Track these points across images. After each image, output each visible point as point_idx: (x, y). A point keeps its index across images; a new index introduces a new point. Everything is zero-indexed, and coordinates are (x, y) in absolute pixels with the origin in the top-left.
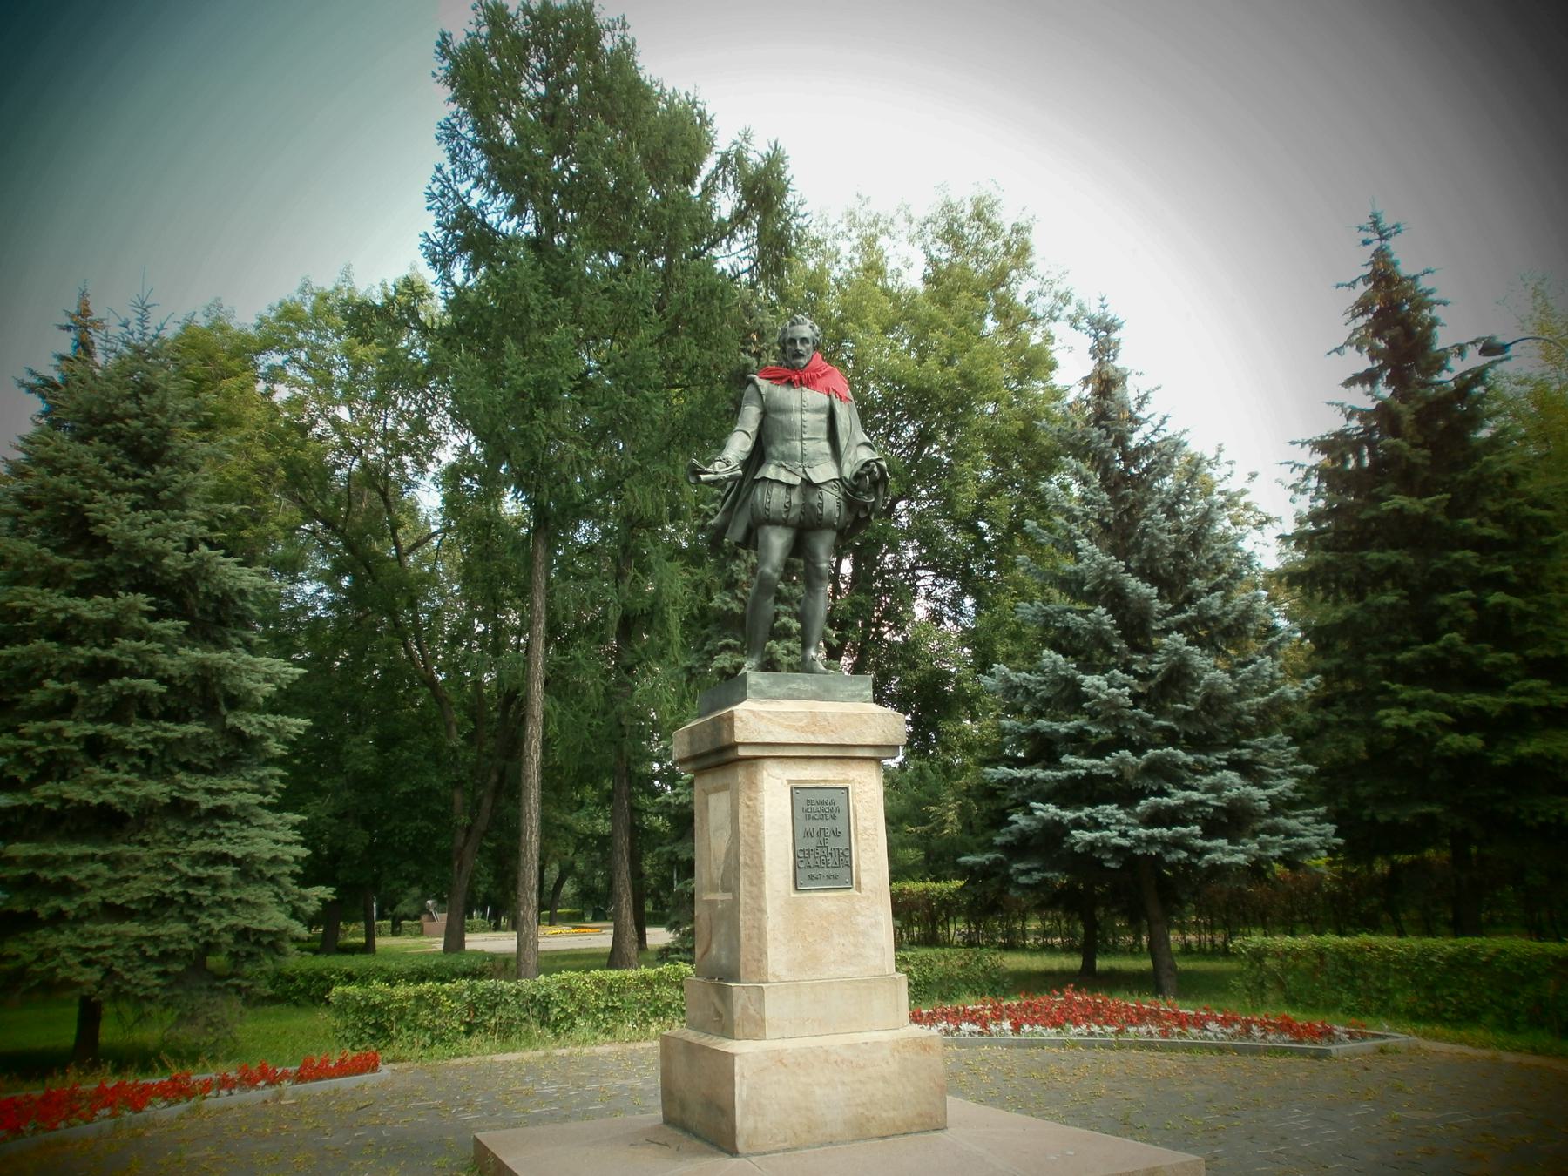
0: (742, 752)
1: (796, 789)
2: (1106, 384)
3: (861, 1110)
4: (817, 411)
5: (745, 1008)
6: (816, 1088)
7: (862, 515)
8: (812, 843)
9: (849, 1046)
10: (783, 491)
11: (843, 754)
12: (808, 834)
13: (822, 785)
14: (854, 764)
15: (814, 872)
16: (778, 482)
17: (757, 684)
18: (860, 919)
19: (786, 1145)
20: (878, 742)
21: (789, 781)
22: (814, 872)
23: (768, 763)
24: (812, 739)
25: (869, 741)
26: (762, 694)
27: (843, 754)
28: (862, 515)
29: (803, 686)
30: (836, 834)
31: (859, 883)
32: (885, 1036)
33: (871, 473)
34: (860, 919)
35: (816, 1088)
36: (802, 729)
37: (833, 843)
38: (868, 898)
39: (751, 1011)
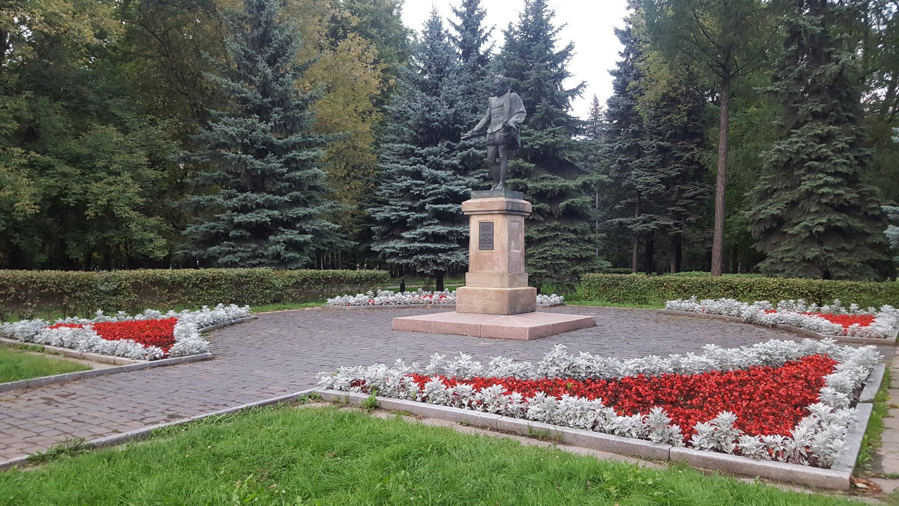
8: (483, 238)
26: (476, 198)
27: (490, 213)
37: (489, 238)
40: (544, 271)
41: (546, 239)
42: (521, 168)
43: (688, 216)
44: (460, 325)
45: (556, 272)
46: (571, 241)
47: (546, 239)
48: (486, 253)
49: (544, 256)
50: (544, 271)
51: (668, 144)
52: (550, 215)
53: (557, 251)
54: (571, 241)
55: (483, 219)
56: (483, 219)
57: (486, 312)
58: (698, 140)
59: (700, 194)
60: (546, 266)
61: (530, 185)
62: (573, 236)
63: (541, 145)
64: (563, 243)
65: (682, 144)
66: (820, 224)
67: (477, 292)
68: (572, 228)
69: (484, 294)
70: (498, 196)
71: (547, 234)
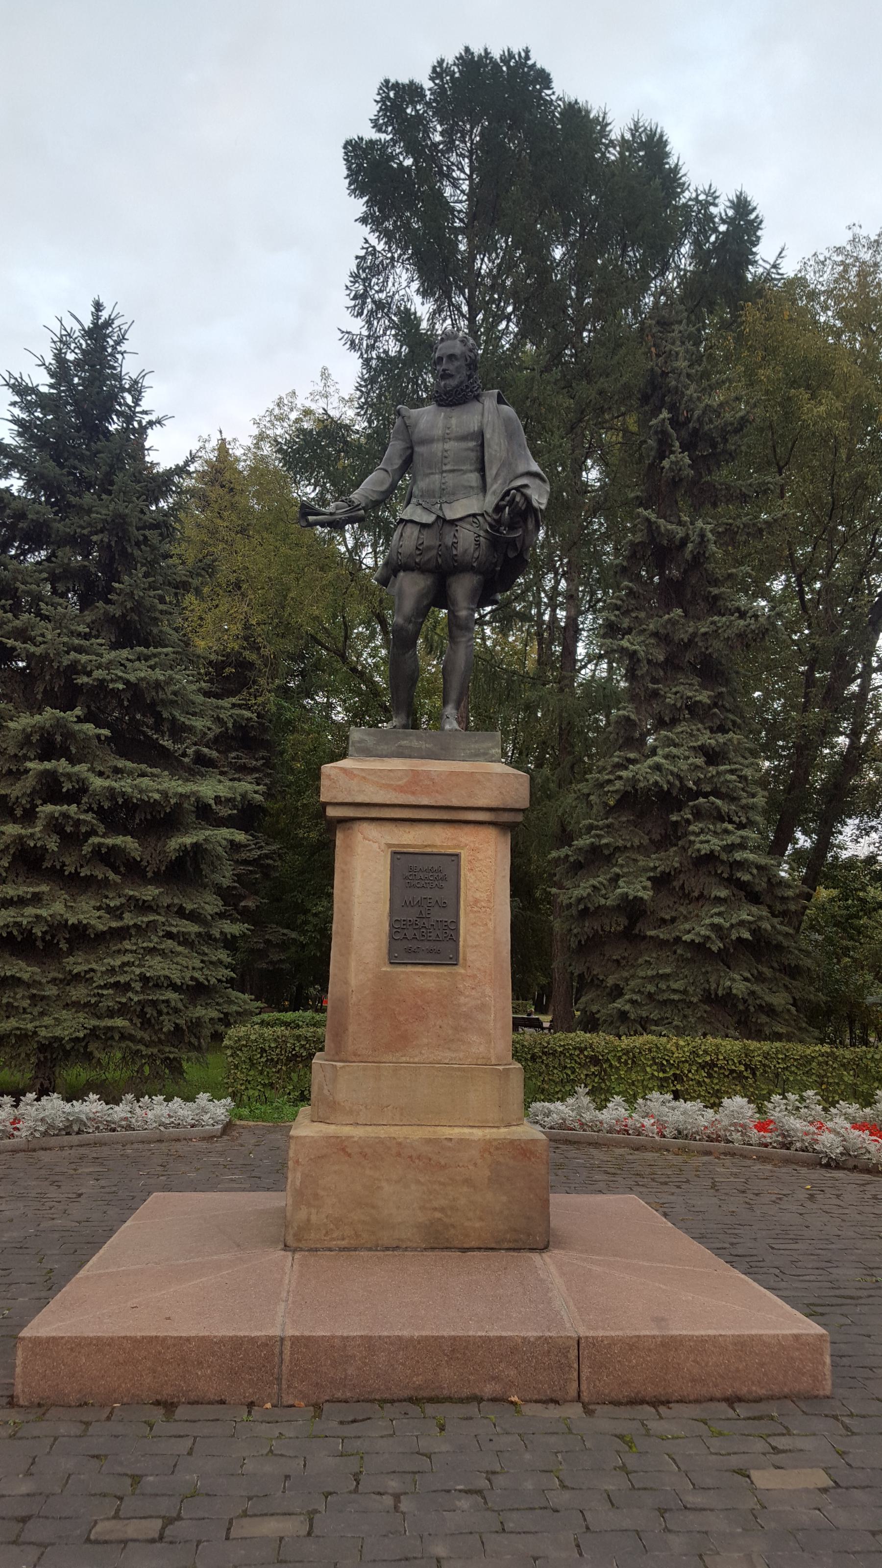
0: (331, 812)
1: (398, 856)
2: (677, 165)
3: (438, 1215)
4: (464, 438)
5: (321, 1088)
6: (384, 1184)
7: (512, 555)
8: (411, 914)
9: (429, 1141)
10: (416, 530)
11: (452, 816)
12: (406, 904)
13: (429, 850)
14: (468, 829)
15: (414, 945)
16: (412, 521)
17: (361, 741)
18: (462, 1000)
19: (343, 1243)
20: (494, 804)
21: (389, 846)
22: (414, 945)
23: (365, 827)
24: (425, 801)
25: (482, 803)
26: (367, 752)
27: (452, 816)
28: (512, 555)
29: (415, 744)
30: (444, 906)
31: (465, 960)
32: (478, 1133)
33: (512, 501)
34: (462, 1000)
35: (384, 1184)
36: (401, 789)
37: (437, 915)
38: (474, 977)
39: (326, 1092)
40: (119, 1022)
41: (122, 933)
42: (69, 735)
43: (244, 898)
44: (458, 1349)
45: (146, 1023)
46: (184, 940)
47: (122, 933)
48: (424, 978)
49: (122, 979)
50: (119, 1022)
51: (215, 754)
52: (133, 870)
53: (157, 967)
54: (184, 940)
55: (412, 838)
56: (412, 838)
57: (441, 1240)
58: (263, 753)
59: (267, 856)
60: (123, 1010)
61: (98, 783)
62: (194, 929)
63: (127, 683)
64: (169, 944)
65: (237, 757)
66: (742, 923)
67: (397, 1150)
68: (189, 906)
69: (431, 1161)
70: (475, 756)
71: (129, 919)
